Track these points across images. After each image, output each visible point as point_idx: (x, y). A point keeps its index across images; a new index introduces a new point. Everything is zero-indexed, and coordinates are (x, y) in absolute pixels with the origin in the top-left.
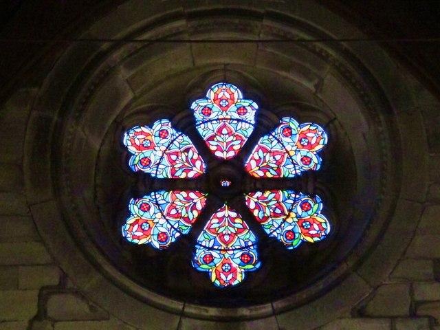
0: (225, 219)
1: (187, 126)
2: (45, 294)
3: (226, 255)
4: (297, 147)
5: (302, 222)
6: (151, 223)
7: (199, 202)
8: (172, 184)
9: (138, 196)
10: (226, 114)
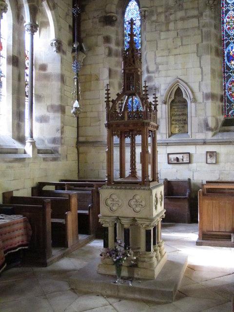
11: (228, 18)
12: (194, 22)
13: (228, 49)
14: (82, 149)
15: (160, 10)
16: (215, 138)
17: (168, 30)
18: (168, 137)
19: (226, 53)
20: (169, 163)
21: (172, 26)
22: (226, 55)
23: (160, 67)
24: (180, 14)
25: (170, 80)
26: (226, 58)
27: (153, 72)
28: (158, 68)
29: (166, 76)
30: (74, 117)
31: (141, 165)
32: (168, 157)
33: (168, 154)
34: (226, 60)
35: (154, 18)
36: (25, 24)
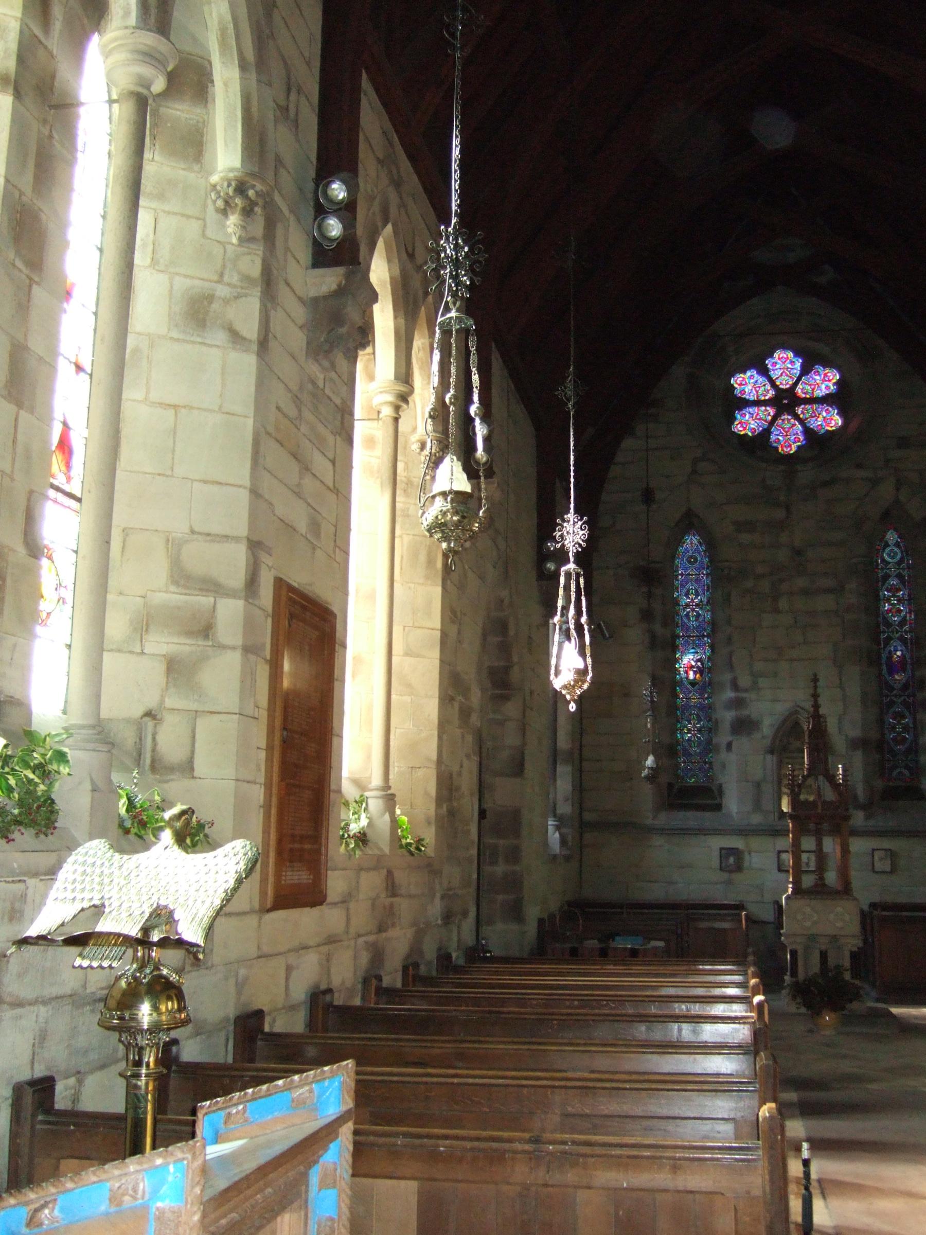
0: (784, 382)
1: (764, 371)
2: (695, 461)
3: (788, 437)
4: (824, 381)
5: (830, 420)
6: (748, 423)
7: (772, 411)
8: (758, 403)
9: (740, 409)
10: (784, 365)
11: (899, 611)
12: (824, 603)
13: (888, 649)
14: (588, 837)
15: (760, 570)
16: (871, 823)
17: (776, 611)
18: (776, 819)
19: (884, 656)
20: (780, 870)
21: (783, 604)
22: (883, 661)
23: (760, 680)
24: (801, 582)
25: (782, 708)
26: (884, 667)
27: (746, 691)
28: (755, 683)
29: (775, 700)
30: (425, 536)
31: (460, 463)
32: (778, 857)
33: (779, 852)
34: (885, 671)
35: (749, 584)
36: (222, 175)
